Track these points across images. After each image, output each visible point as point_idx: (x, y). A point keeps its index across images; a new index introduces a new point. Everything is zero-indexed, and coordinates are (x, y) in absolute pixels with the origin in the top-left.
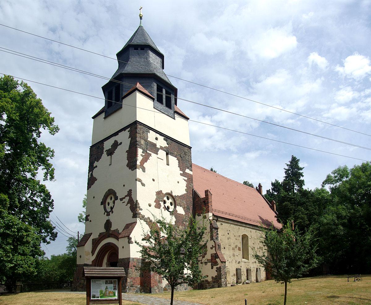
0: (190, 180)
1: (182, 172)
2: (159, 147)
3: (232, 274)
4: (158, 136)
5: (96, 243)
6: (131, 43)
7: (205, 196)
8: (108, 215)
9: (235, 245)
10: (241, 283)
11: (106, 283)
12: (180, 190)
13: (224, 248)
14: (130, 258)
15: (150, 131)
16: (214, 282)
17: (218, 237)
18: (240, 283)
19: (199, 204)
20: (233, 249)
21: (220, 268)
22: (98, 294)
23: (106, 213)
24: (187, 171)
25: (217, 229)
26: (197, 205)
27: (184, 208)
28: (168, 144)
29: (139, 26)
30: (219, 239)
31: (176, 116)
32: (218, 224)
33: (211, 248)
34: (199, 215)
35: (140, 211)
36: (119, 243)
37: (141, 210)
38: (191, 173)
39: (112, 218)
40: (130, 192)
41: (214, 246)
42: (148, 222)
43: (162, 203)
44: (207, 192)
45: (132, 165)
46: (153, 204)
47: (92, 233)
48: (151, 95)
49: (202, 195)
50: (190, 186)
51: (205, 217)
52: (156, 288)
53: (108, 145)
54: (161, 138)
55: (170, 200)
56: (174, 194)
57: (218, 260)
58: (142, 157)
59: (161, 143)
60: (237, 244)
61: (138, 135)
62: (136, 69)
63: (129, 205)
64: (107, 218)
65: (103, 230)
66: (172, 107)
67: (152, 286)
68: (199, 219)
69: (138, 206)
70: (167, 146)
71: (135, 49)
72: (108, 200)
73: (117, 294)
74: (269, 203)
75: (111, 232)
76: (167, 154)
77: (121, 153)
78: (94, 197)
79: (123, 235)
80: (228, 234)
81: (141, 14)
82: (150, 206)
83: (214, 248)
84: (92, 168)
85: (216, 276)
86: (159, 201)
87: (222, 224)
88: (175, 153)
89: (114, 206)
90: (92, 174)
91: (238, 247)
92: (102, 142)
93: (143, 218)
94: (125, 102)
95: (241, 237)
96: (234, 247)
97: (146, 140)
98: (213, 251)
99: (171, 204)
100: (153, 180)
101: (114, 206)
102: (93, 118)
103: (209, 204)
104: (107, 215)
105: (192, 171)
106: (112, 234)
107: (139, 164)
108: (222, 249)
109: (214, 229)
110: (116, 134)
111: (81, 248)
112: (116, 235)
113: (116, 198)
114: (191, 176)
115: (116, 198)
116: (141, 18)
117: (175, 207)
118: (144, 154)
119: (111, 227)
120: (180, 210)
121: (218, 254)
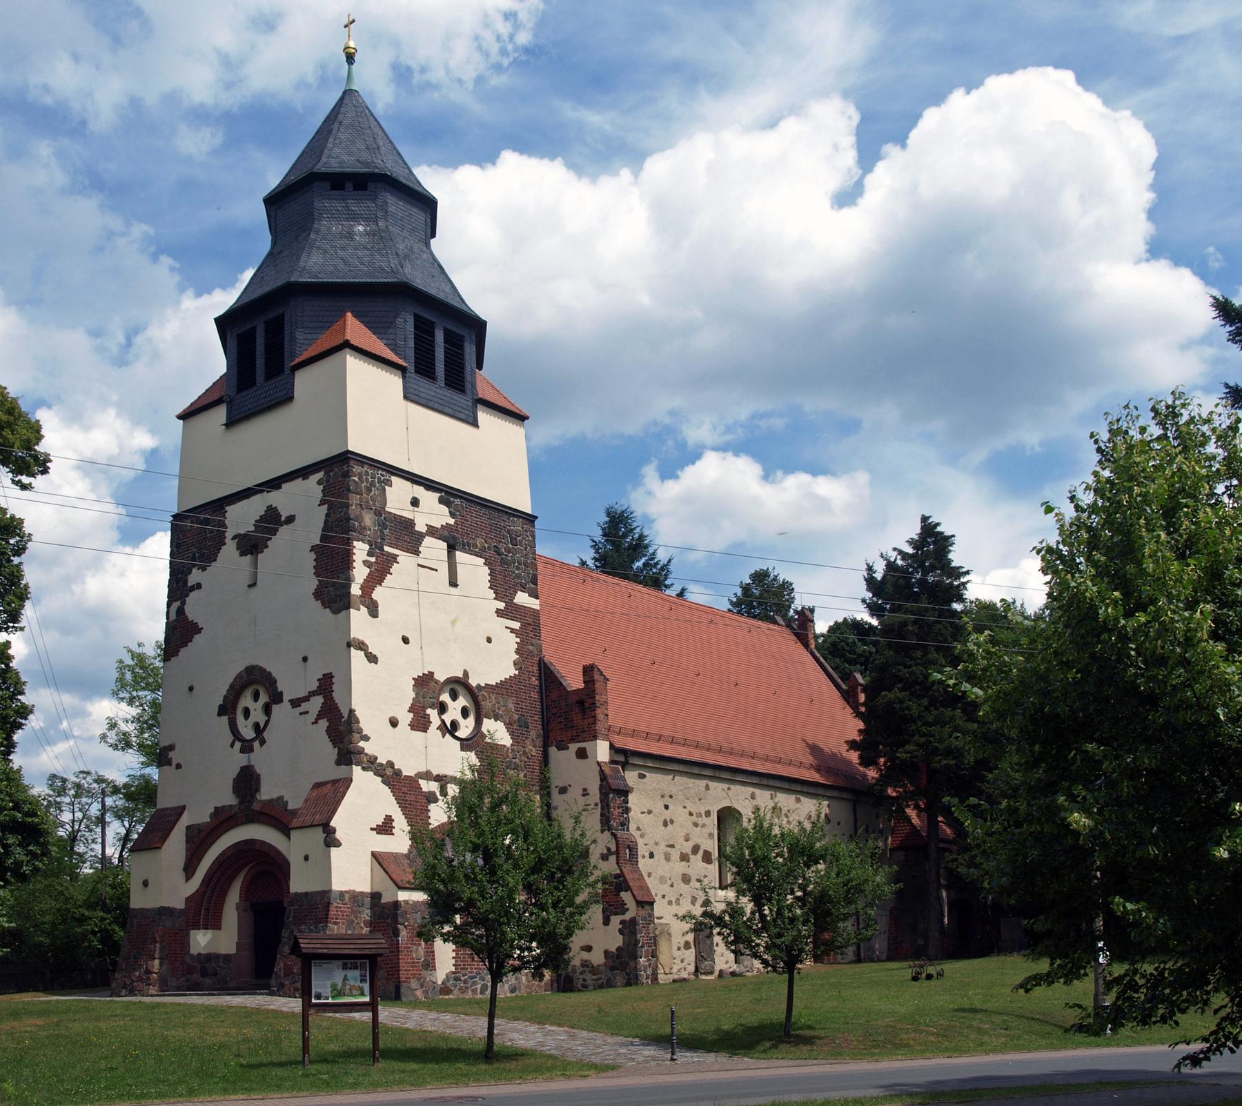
0: (529, 628)
1: (502, 605)
2: (423, 529)
3: (678, 940)
4: (420, 491)
5: (199, 840)
6: (321, 167)
7: (582, 686)
8: (247, 748)
9: (690, 844)
10: (712, 973)
11: (345, 967)
12: (495, 662)
13: (652, 855)
14: (330, 891)
15: (394, 479)
16: (612, 968)
17: (628, 819)
18: (707, 973)
19: (557, 707)
20: (684, 858)
21: (633, 921)
22: (327, 991)
23: (238, 745)
24: (522, 598)
25: (625, 792)
26: (555, 711)
27: (508, 726)
28: (452, 515)
29: (345, 92)
30: (632, 827)
31: (483, 416)
32: (631, 777)
33: (604, 857)
34: (562, 747)
35: (362, 744)
36: (294, 847)
37: (366, 738)
38: (534, 603)
39: (260, 759)
40: (326, 685)
41: (614, 849)
42: (391, 776)
43: (433, 713)
44: (589, 671)
45: (334, 595)
46: (406, 718)
47: (184, 808)
48: (396, 354)
49: (574, 681)
50: (531, 648)
51: (582, 754)
52: (414, 984)
53: (242, 518)
54: (430, 499)
55: (462, 701)
56: (473, 682)
57: (626, 896)
58: (368, 570)
59: (431, 513)
60: (698, 841)
61: (354, 499)
62: (341, 266)
63: (324, 724)
64: (243, 760)
65: (227, 798)
66: (468, 386)
67: (403, 977)
68: (563, 761)
69: (354, 726)
70: (452, 521)
71: (333, 188)
72: (246, 701)
73: (367, 991)
74: (834, 674)
75: (256, 806)
76: (452, 548)
77: (294, 549)
78: (191, 689)
79: (308, 820)
80: (666, 807)
81: (352, 44)
82: (394, 723)
83: (613, 858)
84: (179, 588)
85: (619, 949)
86: (424, 708)
87: (642, 776)
88: (479, 542)
89: (267, 723)
90: (181, 611)
91: (701, 853)
92: (219, 505)
93: (371, 764)
94: (304, 382)
95: (714, 816)
96: (689, 851)
97: (380, 512)
98: (610, 867)
99: (465, 713)
100: (406, 640)
101: (267, 723)
102: (185, 416)
103: (598, 711)
104: (242, 751)
105: (537, 598)
106: (260, 813)
107: (359, 593)
108: (644, 857)
109: (612, 795)
110: (274, 484)
111: (146, 857)
112: (279, 817)
113: (277, 698)
114: (535, 613)
115: (277, 698)
116: (350, 58)
117: (479, 723)
118: (373, 559)
119: (258, 790)
120: (498, 732)
121: (629, 876)
